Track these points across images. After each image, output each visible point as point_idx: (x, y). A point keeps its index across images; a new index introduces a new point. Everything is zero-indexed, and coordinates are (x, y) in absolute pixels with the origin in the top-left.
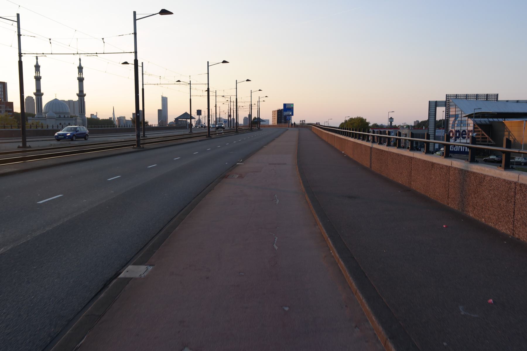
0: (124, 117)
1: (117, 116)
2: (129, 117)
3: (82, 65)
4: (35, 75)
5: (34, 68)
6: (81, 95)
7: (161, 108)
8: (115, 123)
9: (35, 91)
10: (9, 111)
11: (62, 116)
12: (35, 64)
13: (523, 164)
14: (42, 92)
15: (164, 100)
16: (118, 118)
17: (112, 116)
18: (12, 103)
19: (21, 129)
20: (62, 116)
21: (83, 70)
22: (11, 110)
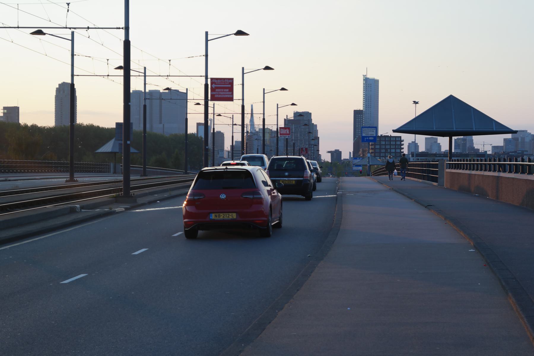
15: (371, 88)
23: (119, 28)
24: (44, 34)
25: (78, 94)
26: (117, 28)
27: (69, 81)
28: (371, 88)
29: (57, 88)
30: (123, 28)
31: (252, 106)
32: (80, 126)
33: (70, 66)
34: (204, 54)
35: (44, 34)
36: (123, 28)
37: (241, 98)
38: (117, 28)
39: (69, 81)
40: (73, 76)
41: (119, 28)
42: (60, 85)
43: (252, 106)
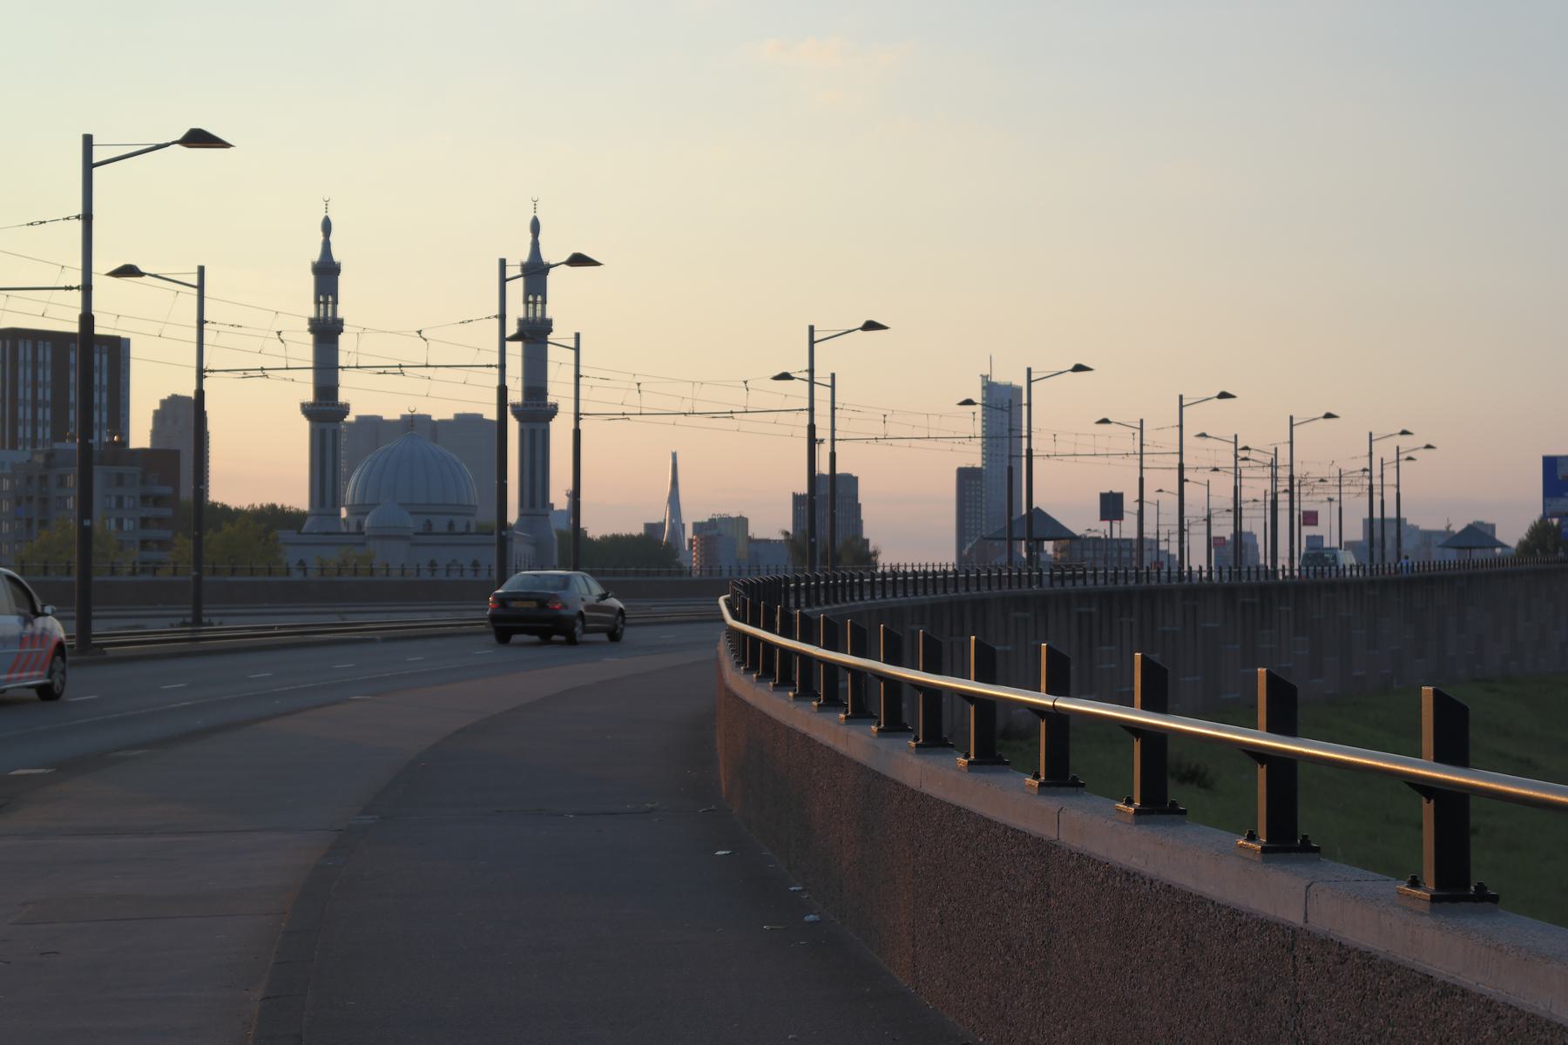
0: (742, 522)
1: (695, 512)
2: (772, 520)
3: (337, 256)
4: (312, 314)
5: (310, 280)
6: (200, 393)
7: (973, 456)
8: (681, 558)
9: (309, 396)
10: (158, 501)
11: (440, 524)
12: (316, 255)
13: (87, 523)
14: (551, 399)
15: (1003, 409)
16: (698, 527)
17: (660, 514)
18: (1120, 495)
19: (74, 578)
20: (440, 524)
21: (342, 279)
22: (167, 490)
23: (71, 288)
24: (142, 274)
25: (212, 426)
26: (66, 288)
27: (190, 392)
28: (1003, 409)
29: (156, 413)
30: (87, 319)
31: (674, 456)
32: (225, 513)
33: (194, 347)
34: (497, 312)
35: (142, 274)
36: (87, 319)
37: (496, 361)
38: (66, 288)
39: (190, 392)
40: (201, 373)
41: (71, 288)
42: (163, 402)
43: (674, 456)
